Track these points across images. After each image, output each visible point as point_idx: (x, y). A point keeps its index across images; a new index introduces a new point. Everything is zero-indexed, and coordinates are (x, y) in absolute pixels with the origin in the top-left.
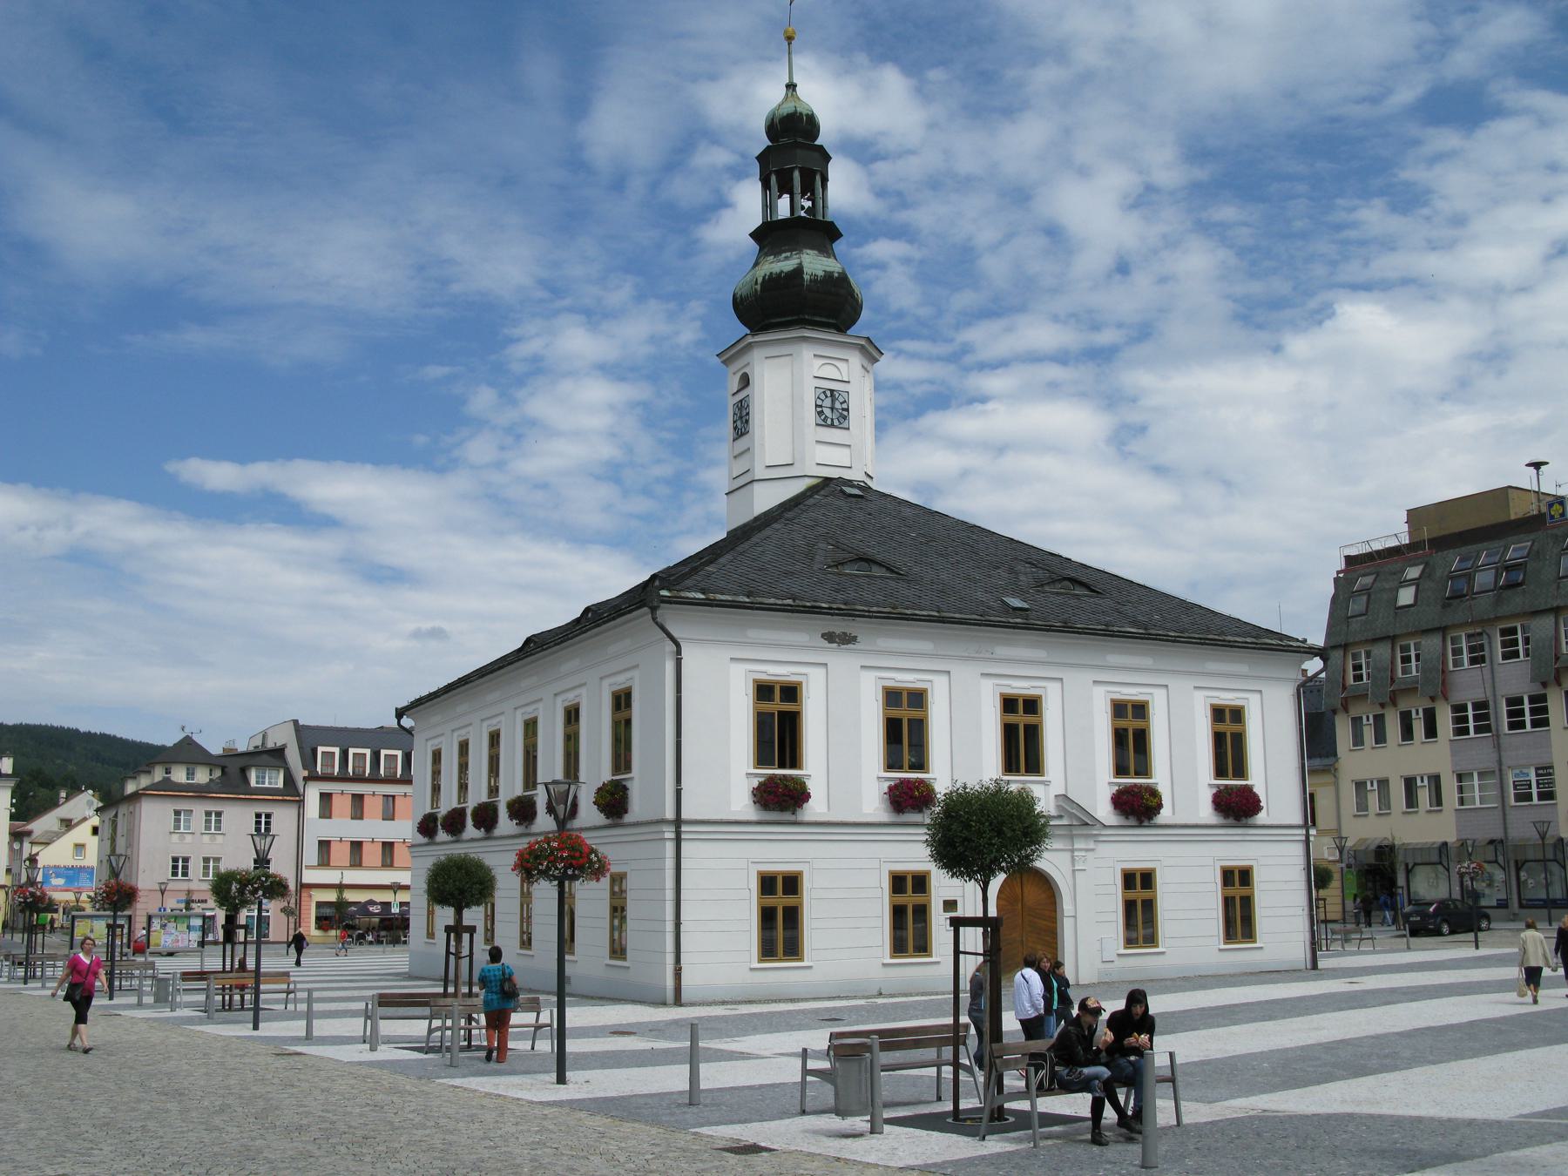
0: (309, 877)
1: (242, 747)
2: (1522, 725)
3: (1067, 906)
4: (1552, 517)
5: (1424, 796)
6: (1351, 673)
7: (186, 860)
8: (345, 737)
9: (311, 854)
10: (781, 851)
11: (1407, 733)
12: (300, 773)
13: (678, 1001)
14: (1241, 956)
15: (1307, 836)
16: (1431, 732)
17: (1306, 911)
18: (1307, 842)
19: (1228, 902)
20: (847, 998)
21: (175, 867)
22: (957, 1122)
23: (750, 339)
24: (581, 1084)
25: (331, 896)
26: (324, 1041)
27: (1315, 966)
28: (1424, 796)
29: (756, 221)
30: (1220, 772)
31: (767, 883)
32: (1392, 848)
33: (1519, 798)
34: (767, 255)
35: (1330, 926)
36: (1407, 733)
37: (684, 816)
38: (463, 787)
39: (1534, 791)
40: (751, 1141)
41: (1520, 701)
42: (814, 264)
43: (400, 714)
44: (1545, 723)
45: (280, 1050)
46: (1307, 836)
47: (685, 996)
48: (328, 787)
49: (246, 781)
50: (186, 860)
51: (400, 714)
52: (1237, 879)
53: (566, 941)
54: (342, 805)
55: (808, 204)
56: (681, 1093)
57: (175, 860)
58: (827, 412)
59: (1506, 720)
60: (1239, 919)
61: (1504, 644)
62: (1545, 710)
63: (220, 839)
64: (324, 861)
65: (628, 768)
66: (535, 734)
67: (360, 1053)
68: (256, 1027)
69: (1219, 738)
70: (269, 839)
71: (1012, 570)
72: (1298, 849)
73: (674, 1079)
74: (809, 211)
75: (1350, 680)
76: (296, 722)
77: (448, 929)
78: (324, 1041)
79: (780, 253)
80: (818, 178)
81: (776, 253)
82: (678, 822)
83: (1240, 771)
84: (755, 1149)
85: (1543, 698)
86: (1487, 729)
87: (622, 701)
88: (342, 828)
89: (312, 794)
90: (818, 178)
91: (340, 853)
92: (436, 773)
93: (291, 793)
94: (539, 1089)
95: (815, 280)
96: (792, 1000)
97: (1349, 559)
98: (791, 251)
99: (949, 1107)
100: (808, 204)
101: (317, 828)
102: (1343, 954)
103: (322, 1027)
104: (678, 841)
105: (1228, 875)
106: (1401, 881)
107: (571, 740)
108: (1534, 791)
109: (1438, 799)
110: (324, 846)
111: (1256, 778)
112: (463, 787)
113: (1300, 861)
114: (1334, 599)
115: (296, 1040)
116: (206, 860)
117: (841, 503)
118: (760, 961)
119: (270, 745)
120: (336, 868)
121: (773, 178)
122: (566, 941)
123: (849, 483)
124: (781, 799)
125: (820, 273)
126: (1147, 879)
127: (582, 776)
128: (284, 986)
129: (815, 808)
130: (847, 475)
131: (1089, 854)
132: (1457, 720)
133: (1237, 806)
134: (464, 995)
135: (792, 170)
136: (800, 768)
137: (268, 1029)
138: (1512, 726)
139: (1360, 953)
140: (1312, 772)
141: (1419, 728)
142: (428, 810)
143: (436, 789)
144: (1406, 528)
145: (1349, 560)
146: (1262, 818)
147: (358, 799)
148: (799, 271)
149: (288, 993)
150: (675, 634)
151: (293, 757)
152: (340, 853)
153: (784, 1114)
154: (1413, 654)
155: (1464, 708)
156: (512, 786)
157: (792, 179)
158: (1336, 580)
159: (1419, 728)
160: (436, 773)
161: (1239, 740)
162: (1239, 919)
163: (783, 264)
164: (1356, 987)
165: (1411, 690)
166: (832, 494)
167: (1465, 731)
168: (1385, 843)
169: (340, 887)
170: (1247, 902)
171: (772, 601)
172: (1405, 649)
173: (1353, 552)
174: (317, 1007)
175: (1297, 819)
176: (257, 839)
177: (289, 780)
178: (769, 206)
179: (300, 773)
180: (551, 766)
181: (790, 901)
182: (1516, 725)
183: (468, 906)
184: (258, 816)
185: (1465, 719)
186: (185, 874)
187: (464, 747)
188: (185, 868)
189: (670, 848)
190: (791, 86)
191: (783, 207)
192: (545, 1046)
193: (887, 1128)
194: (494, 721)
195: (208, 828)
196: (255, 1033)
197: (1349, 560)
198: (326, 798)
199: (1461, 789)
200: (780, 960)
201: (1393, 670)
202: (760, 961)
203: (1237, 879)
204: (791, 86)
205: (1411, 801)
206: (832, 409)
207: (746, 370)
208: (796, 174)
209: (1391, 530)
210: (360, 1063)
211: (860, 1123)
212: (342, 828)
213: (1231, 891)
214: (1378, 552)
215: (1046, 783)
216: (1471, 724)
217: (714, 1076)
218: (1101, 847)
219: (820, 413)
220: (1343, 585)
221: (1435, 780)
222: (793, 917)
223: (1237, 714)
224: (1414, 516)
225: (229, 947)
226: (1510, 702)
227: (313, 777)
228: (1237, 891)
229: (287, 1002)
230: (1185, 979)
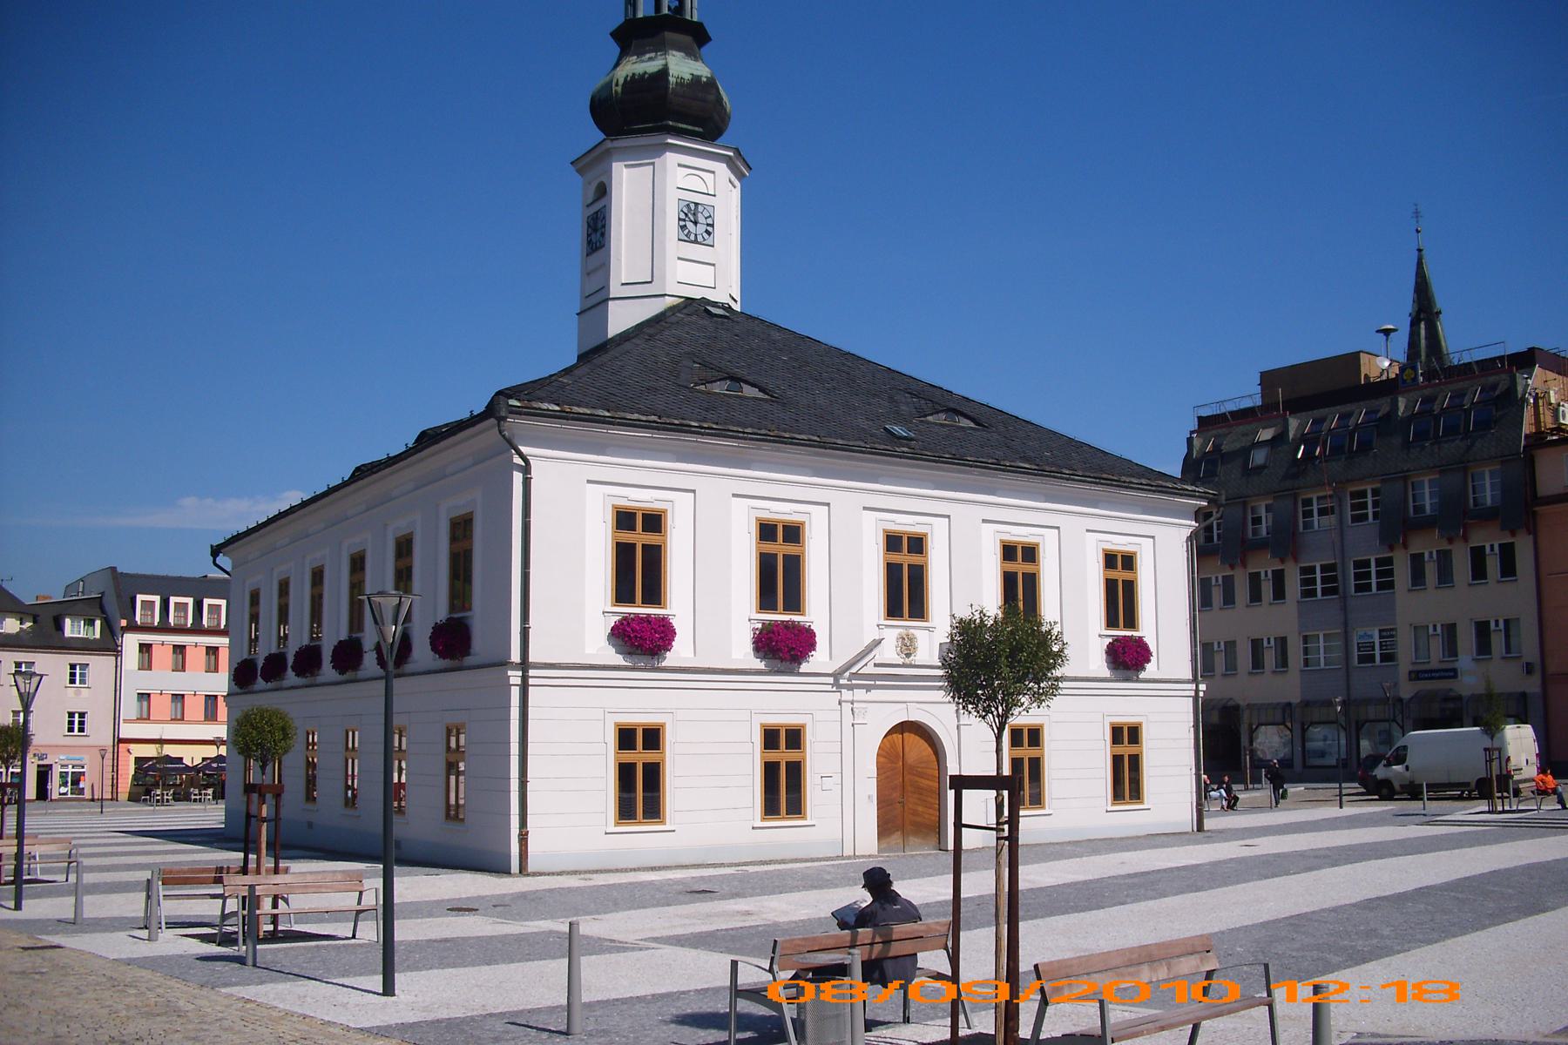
0: (127, 731)
2: (1368, 587)
4: (1404, 381)
5: (1270, 658)
7: (82, 715)
9: (130, 707)
10: (641, 698)
11: (1256, 596)
15: (1197, 691)
16: (1279, 593)
21: (71, 723)
23: (609, 144)
25: (150, 751)
27: (1200, 828)
28: (1270, 658)
29: (621, 20)
30: (1111, 622)
32: (1237, 708)
33: (1362, 659)
36: (1256, 596)
39: (1377, 652)
41: (1367, 564)
42: (681, 67)
44: (1391, 585)
46: (1197, 691)
47: (532, 866)
49: (60, 627)
50: (82, 715)
51: (216, 551)
52: (1126, 735)
54: (162, 656)
57: (71, 715)
59: (1353, 582)
60: (1127, 779)
61: (1354, 507)
62: (1390, 573)
68: (18, 907)
70: (35, 680)
71: (891, 399)
76: (113, 569)
79: (644, 53)
81: (640, 54)
82: (525, 665)
83: (1131, 622)
85: (1389, 561)
86: (1334, 591)
88: (162, 679)
89: (131, 642)
91: (162, 707)
94: (353, 1003)
97: (1200, 419)
103: (95, 906)
105: (771, 737)
106: (1244, 741)
108: (1377, 652)
109: (1283, 661)
111: (1146, 630)
116: (71, 715)
117: (706, 322)
118: (617, 824)
123: (715, 304)
124: (644, 640)
125: (687, 77)
126: (1134, 733)
129: (680, 652)
132: (1305, 582)
133: (1128, 657)
134: (268, 871)
136: (664, 607)
138: (1359, 588)
141: (1267, 589)
142: (245, 656)
146: (1150, 670)
147: (180, 649)
152: (162, 707)
155: (1312, 570)
156: (334, 631)
159: (1267, 589)
162: (1127, 779)
166: (696, 313)
167: (1312, 593)
168: (1231, 703)
169: (161, 742)
170: (1135, 761)
171: (636, 416)
173: (1206, 413)
176: (20, 679)
182: (1363, 588)
184: (73, 667)
185: (1314, 581)
186: (81, 730)
188: (82, 723)
192: (370, 932)
195: (72, 681)
198: (145, 648)
199: (1306, 651)
203: (1126, 735)
205: (1257, 663)
206: (696, 223)
207: (603, 179)
209: (1247, 393)
210: (129, 962)
212: (162, 679)
213: (1120, 750)
216: (1319, 587)
219: (683, 228)
221: (1282, 642)
222: (653, 774)
224: (1269, 380)
226: (1358, 564)
227: (133, 628)
228: (1126, 750)
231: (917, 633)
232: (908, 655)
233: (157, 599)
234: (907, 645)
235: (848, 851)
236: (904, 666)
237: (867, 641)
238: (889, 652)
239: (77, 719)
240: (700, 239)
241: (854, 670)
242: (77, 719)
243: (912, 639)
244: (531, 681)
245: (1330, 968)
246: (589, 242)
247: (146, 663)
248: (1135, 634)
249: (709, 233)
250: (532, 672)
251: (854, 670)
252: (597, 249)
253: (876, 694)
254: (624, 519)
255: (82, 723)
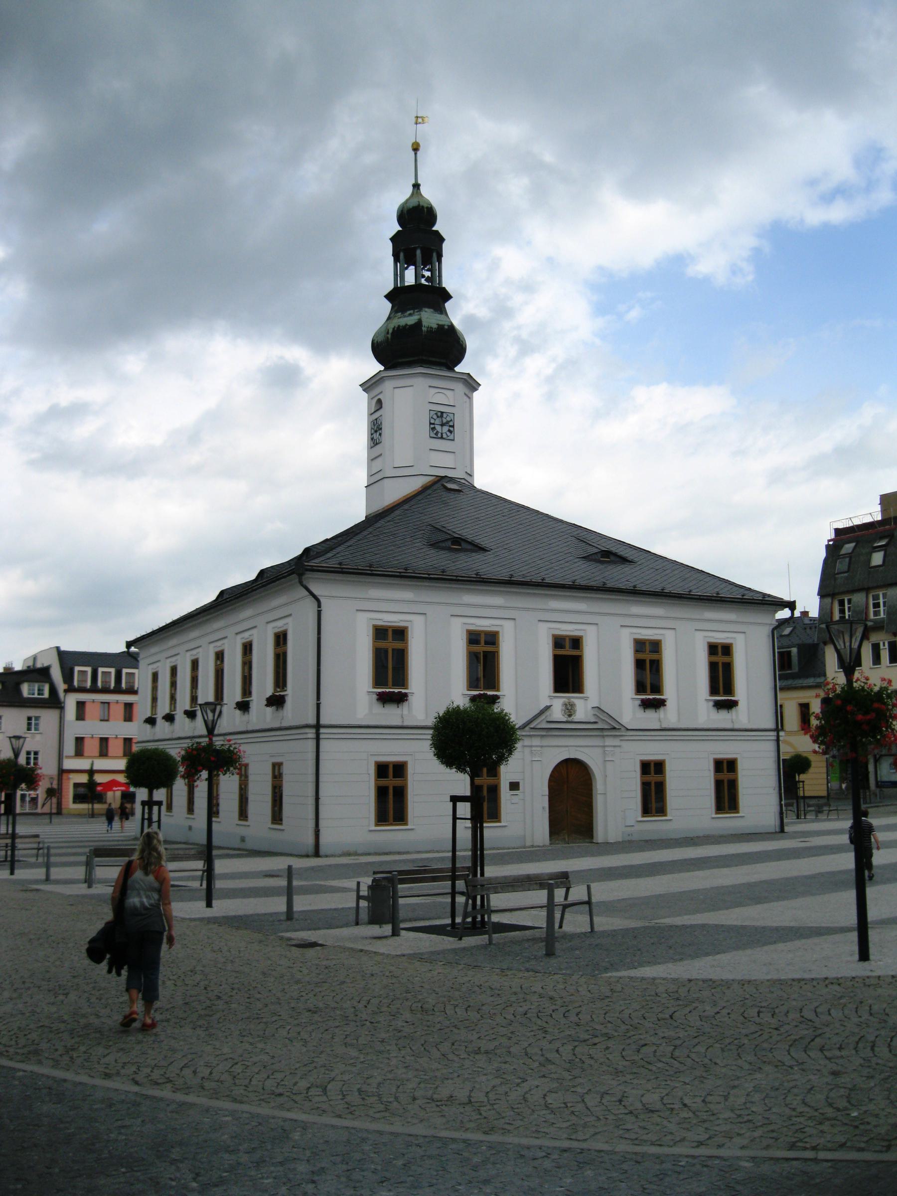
0: (68, 764)
1: (18, 667)
3: (599, 786)
6: (871, 610)
7: (36, 753)
8: (95, 660)
9: (69, 747)
12: (61, 686)
13: (317, 854)
14: (728, 823)
15: (778, 736)
17: (777, 789)
18: (778, 740)
19: (719, 784)
20: (438, 852)
22: (454, 930)
24: (221, 907)
25: (84, 779)
26: (57, 882)
27: (782, 830)
29: (391, 287)
31: (382, 769)
34: (397, 312)
35: (807, 801)
37: (322, 722)
38: (173, 698)
40: (314, 940)
42: (429, 319)
43: (129, 644)
45: (25, 887)
46: (778, 736)
48: (82, 697)
49: (19, 692)
50: (36, 753)
53: (213, 810)
55: (428, 274)
56: (281, 913)
58: (438, 428)
60: (726, 796)
63: (38, 737)
64: (79, 753)
65: (250, 694)
66: (222, 661)
67: (82, 889)
68: (209, 905)
69: (713, 667)
72: (771, 747)
73: (279, 905)
74: (428, 279)
75: (872, 616)
76: (58, 648)
77: (144, 803)
78: (57, 882)
80: (435, 255)
82: (318, 726)
84: (314, 945)
87: (281, 639)
89: (71, 702)
90: (435, 255)
91: (91, 747)
92: (155, 689)
93: (54, 702)
95: (430, 330)
96: (399, 853)
98: (413, 309)
99: (449, 921)
100: (428, 274)
101: (74, 728)
102: (816, 820)
103: (56, 873)
104: (318, 739)
106: (871, 768)
107: (247, 664)
110: (79, 741)
112: (173, 698)
113: (773, 755)
114: (826, 561)
115: (37, 882)
118: (377, 825)
119: (39, 665)
120: (89, 757)
121: (402, 255)
122: (213, 810)
123: (451, 480)
125: (435, 326)
126: (659, 766)
127: (225, 701)
128: (35, 846)
130: (450, 474)
131: (617, 750)
135: (415, 249)
137: (21, 874)
139: (838, 819)
140: (782, 689)
143: (154, 699)
144: (879, 508)
145: (838, 531)
148: (419, 323)
149: (39, 849)
150: (316, 592)
151: (56, 674)
152: (91, 747)
153: (347, 925)
154: (881, 601)
157: (415, 256)
158: (828, 547)
160: (155, 689)
161: (728, 668)
162: (726, 796)
163: (410, 320)
164: (808, 844)
165: (879, 627)
172: (876, 597)
173: (841, 526)
174: (53, 859)
175: (771, 724)
177: (53, 690)
178: (399, 275)
179: (61, 686)
180: (206, 694)
181: (398, 782)
183: (158, 788)
184: (29, 719)
186: (36, 729)
187: (174, 671)
188: (36, 725)
189: (312, 744)
190: (416, 186)
191: (410, 277)
193: (403, 933)
194: (194, 652)
195: (29, 729)
196: (12, 877)
197: (838, 531)
198: (81, 705)
200: (391, 825)
201: (867, 614)
202: (377, 825)
204: (416, 186)
207: (380, 397)
208: (418, 252)
209: (869, 512)
211: (387, 929)
212: (93, 728)
214: (858, 526)
215: (586, 699)
217: (301, 904)
218: (623, 744)
220: (833, 550)
222: (400, 794)
223: (727, 649)
225: (11, 818)
227: (71, 689)
228: (725, 776)
229: (37, 856)
230: (721, 836)
231: (576, 701)
232: (570, 716)
233: (89, 669)
234: (569, 709)
235: (528, 844)
236: (567, 722)
237: (542, 707)
238: (557, 713)
239: (32, 756)
240: (445, 436)
241: (532, 726)
242: (32, 756)
243: (572, 705)
244: (321, 736)
245: (593, 882)
246: (372, 439)
247: (81, 715)
248: (732, 698)
249: (449, 431)
250: (322, 730)
251: (532, 726)
252: (377, 444)
253: (546, 742)
254: (380, 632)
255: (36, 725)
